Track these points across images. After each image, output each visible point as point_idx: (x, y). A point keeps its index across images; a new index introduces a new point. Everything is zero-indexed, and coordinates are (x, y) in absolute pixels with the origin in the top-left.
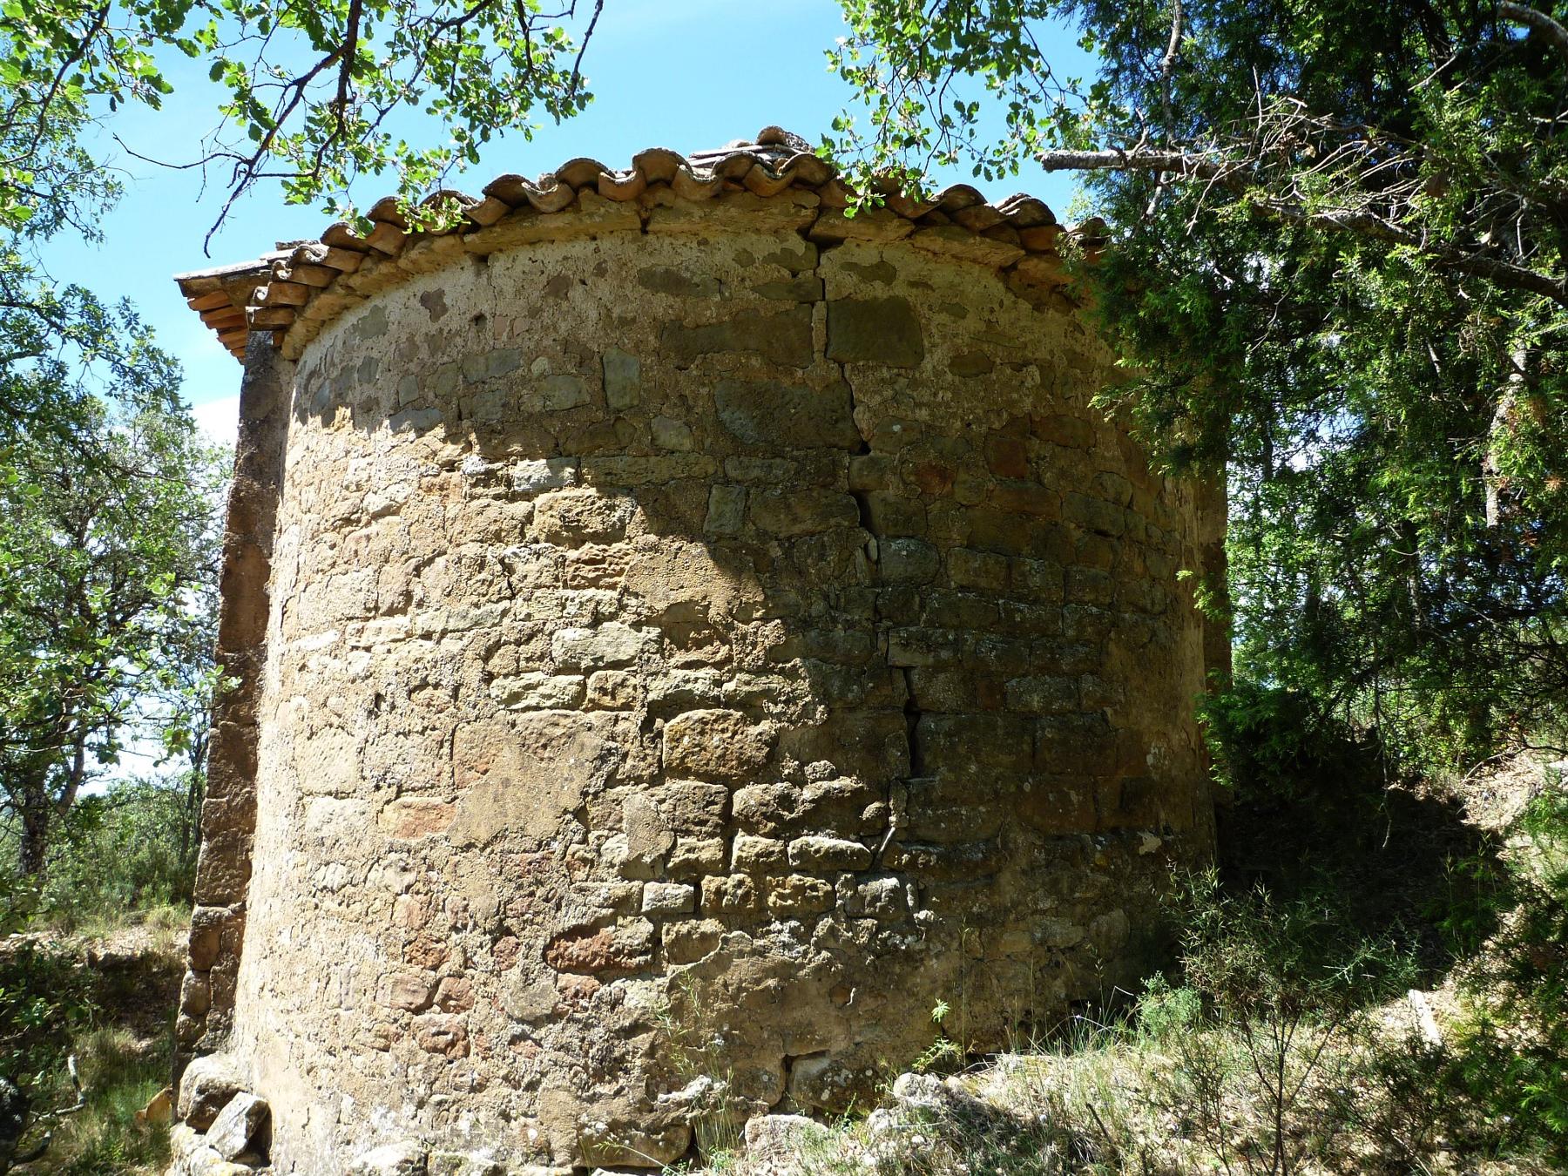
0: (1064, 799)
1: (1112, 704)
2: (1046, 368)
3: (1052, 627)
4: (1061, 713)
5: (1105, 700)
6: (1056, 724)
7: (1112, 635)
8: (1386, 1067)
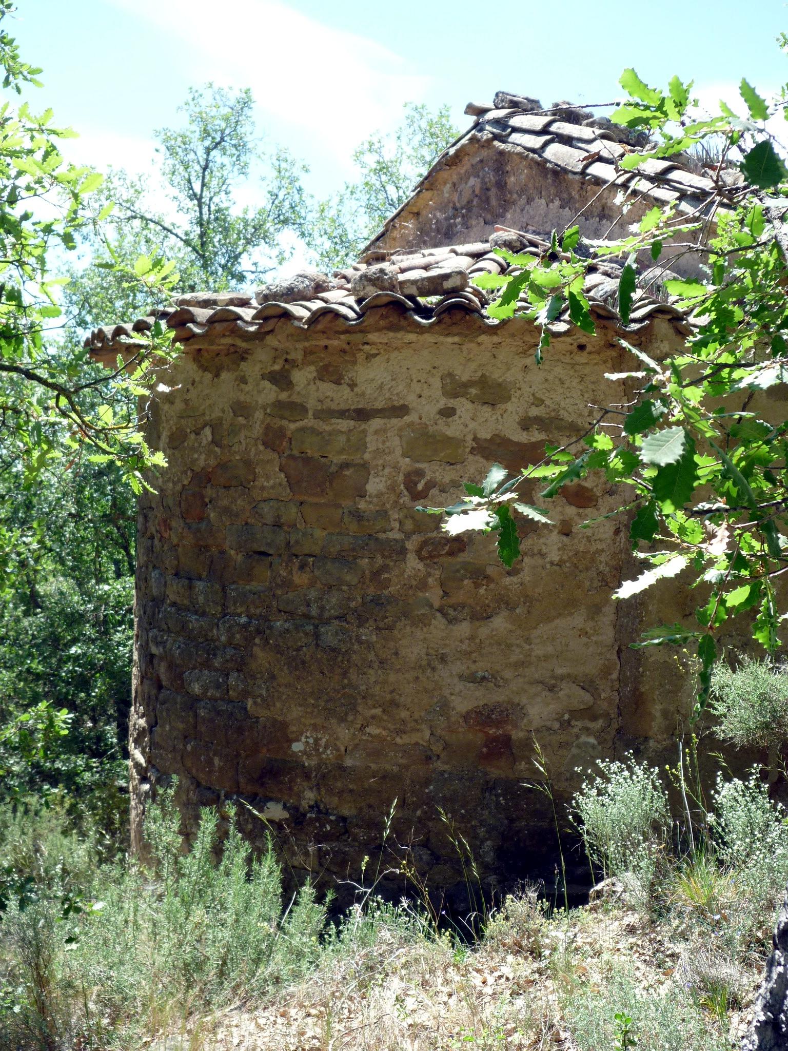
0: (210, 762)
1: (255, 697)
2: (216, 426)
3: (210, 634)
4: (214, 699)
5: (246, 693)
6: (209, 706)
7: (257, 641)
8: (514, 203)
